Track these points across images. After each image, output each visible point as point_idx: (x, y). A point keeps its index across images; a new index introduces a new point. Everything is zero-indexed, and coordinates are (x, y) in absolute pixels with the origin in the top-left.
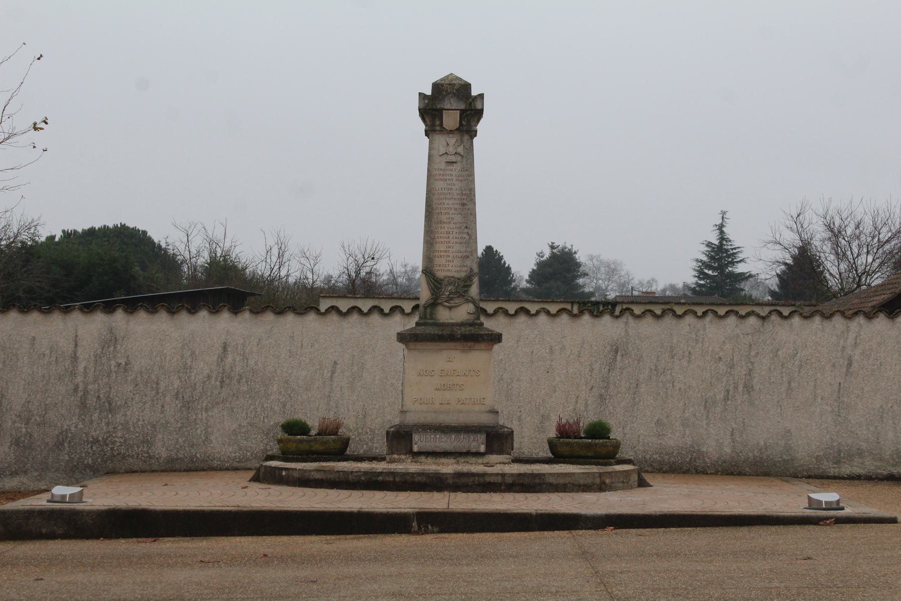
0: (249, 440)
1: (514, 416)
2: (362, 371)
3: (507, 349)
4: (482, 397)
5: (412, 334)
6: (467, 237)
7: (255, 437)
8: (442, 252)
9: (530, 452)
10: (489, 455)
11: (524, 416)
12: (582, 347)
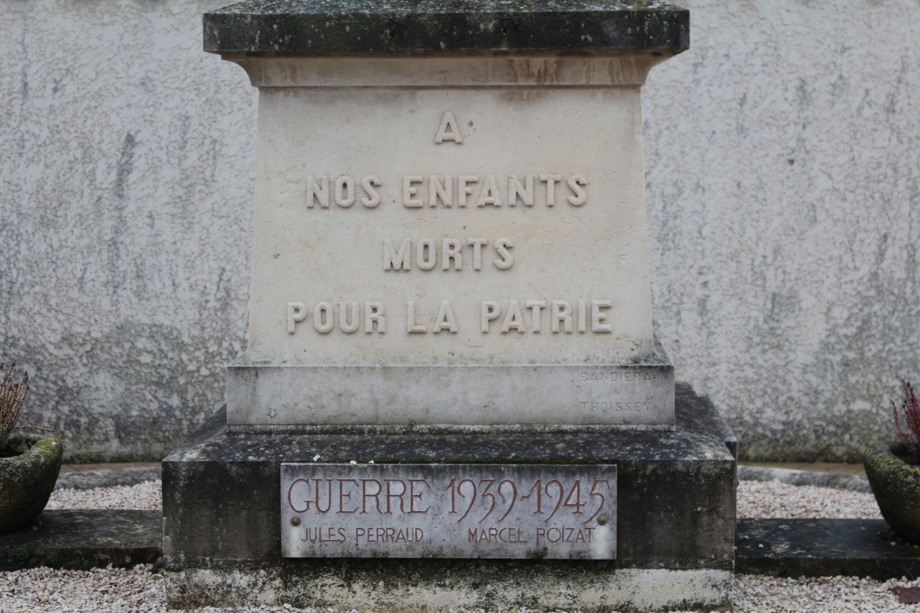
1: (685, 299)
2: (214, 164)
5: (272, 19)
10: (634, 571)
11: (713, 302)
12: (899, 81)
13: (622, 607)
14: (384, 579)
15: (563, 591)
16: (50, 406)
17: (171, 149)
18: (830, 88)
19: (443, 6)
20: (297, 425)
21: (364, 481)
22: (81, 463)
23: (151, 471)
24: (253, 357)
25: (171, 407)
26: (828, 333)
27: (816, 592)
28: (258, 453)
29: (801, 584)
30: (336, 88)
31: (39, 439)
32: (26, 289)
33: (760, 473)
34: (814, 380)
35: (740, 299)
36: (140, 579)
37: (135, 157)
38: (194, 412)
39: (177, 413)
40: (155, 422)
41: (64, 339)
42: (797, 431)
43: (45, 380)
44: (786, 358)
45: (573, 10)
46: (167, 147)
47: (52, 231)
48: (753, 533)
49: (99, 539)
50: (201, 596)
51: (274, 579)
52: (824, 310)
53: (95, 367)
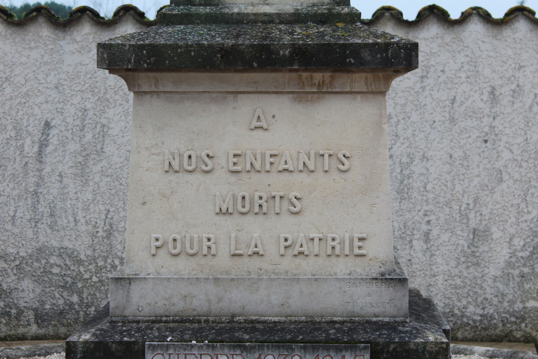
1: (415, 232)
3: (400, 94)
4: (357, 235)
5: (142, 47)
9: (448, 305)
11: (435, 232)
17: (74, 130)
18: (511, 93)
19: (256, 39)
20: (156, 316)
21: (201, 355)
22: (11, 340)
23: (58, 346)
24: (128, 271)
25: (72, 303)
26: (510, 255)
28: (130, 336)
30: (185, 93)
33: (465, 349)
34: (501, 286)
35: (452, 232)
37: (51, 136)
38: (88, 306)
39: (76, 307)
45: (342, 42)
46: (72, 129)
52: (508, 240)
53: (22, 276)
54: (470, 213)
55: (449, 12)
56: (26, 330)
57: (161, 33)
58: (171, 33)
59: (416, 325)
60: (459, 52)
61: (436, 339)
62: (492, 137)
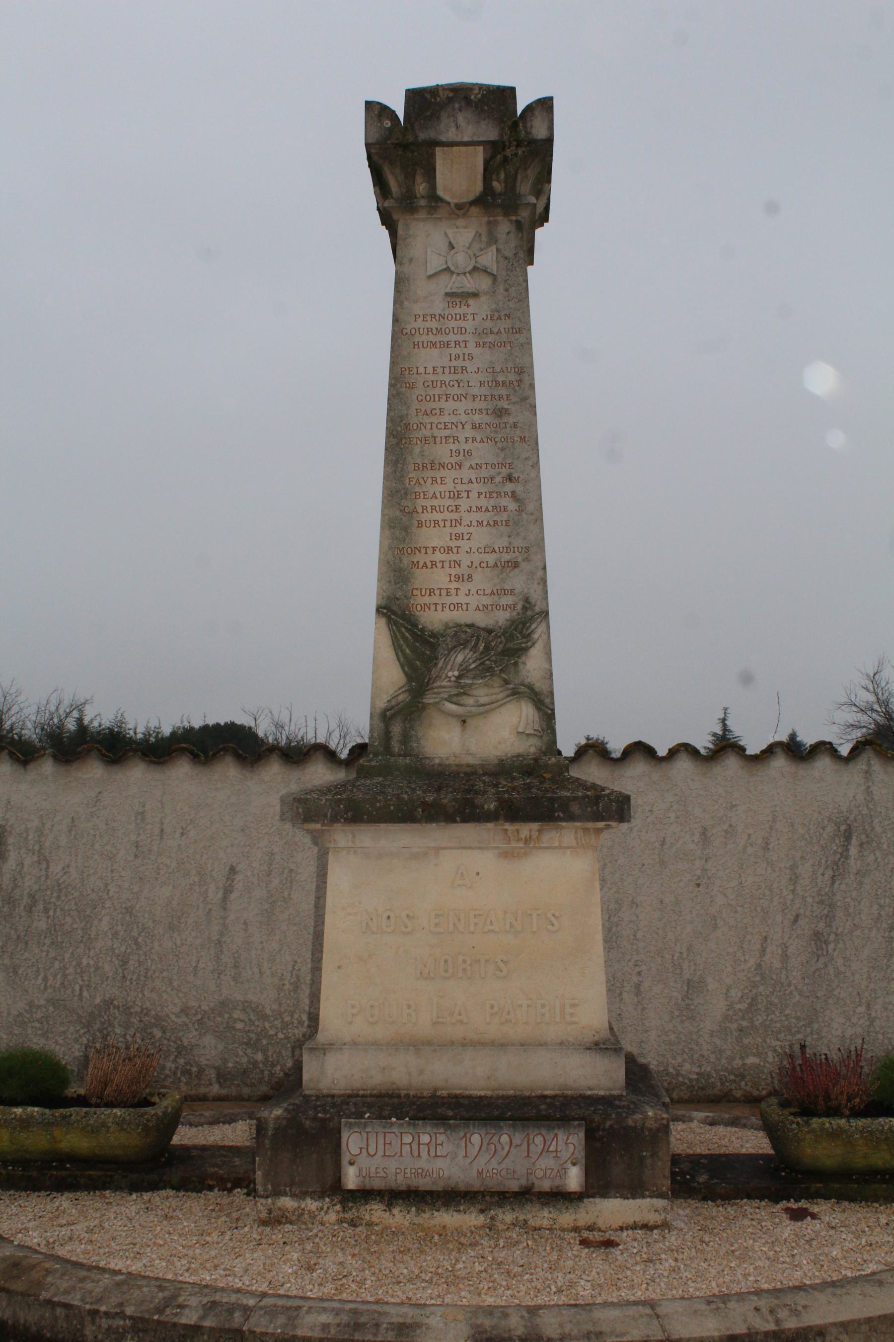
0: (50, 1035)
1: (625, 984)
6: (512, 506)
7: (62, 1029)
8: (437, 552)
10: (598, 1200)
13: (589, 1227)
14: (415, 1206)
15: (546, 1215)
16: (171, 1059)
17: (260, 876)
18: (723, 833)
20: (353, 1090)
21: (401, 1133)
22: (192, 1101)
23: (243, 1113)
25: (257, 1061)
26: (727, 1008)
27: (729, 1212)
28: (325, 1111)
29: (718, 1206)
31: (167, 1093)
32: (157, 974)
33: (683, 1116)
34: (718, 1041)
35: (664, 984)
36: (238, 1201)
37: (236, 881)
38: (273, 1065)
39: (261, 1065)
40: (245, 1072)
41: (182, 1011)
42: (708, 1079)
43: (168, 1040)
44: (698, 1026)
45: (550, 795)
46: (258, 874)
47: (176, 933)
48: (682, 1166)
49: (208, 1169)
50: (282, 1217)
51: (335, 1205)
52: (724, 991)
53: (203, 1031)
54: (683, 962)
55: (656, 749)
56: (208, 1089)
57: (359, 785)
58: (369, 786)
59: (634, 1098)
60: (667, 790)
61: (656, 1114)
62: (705, 881)
